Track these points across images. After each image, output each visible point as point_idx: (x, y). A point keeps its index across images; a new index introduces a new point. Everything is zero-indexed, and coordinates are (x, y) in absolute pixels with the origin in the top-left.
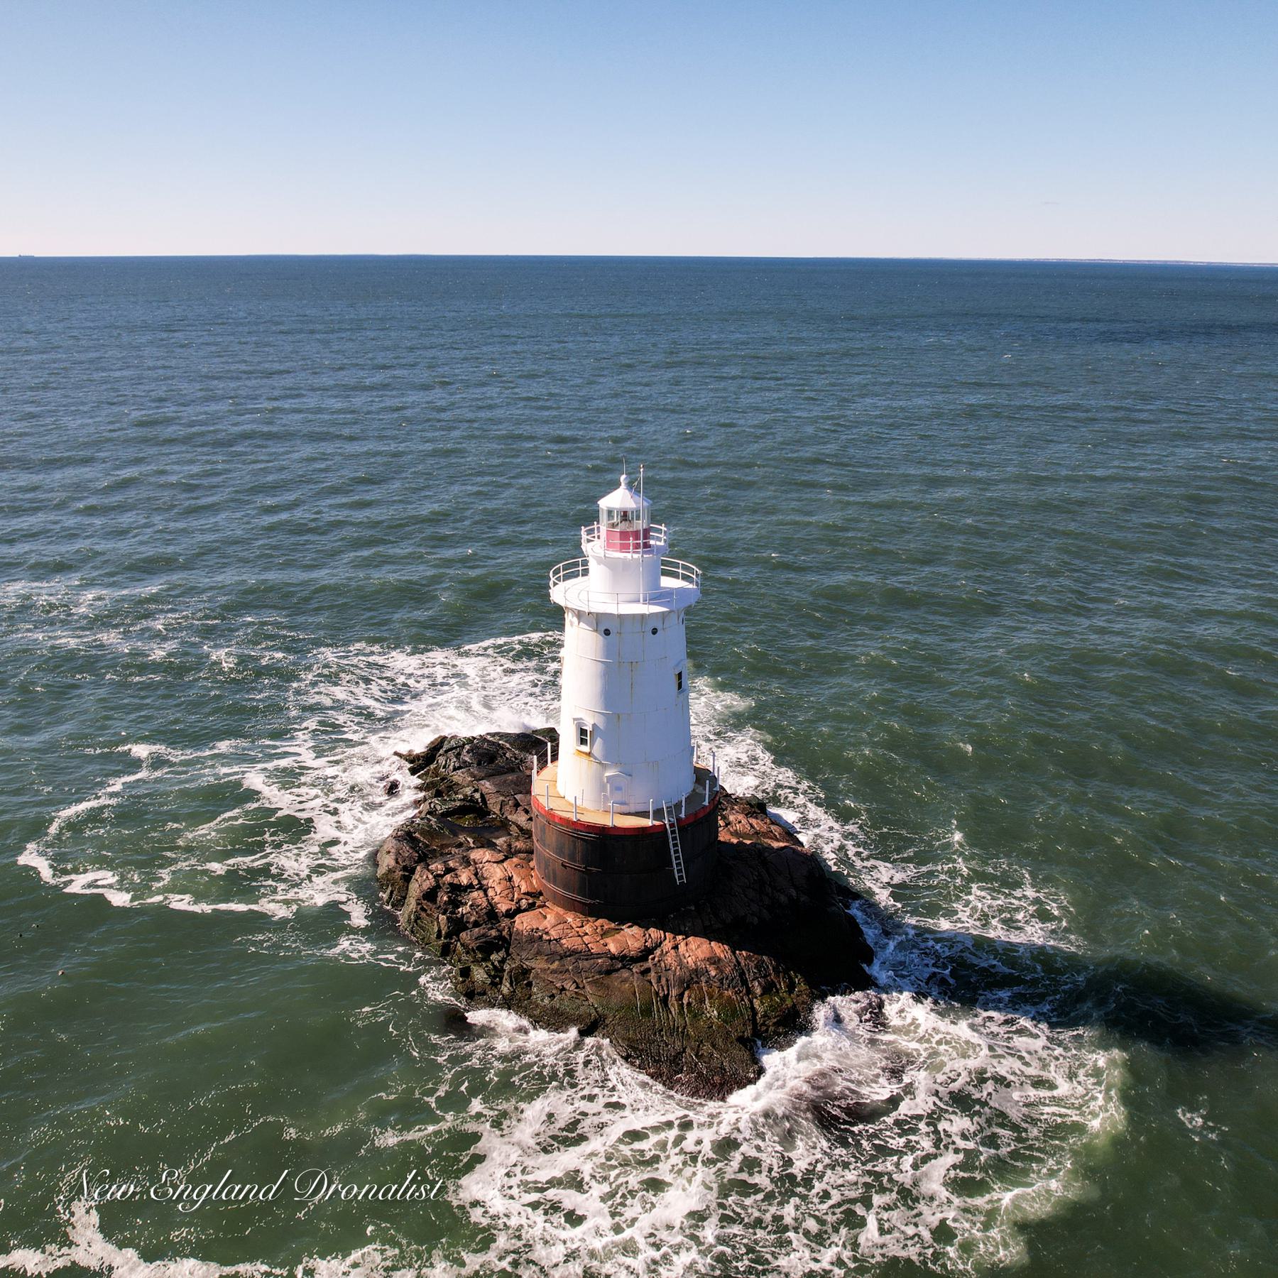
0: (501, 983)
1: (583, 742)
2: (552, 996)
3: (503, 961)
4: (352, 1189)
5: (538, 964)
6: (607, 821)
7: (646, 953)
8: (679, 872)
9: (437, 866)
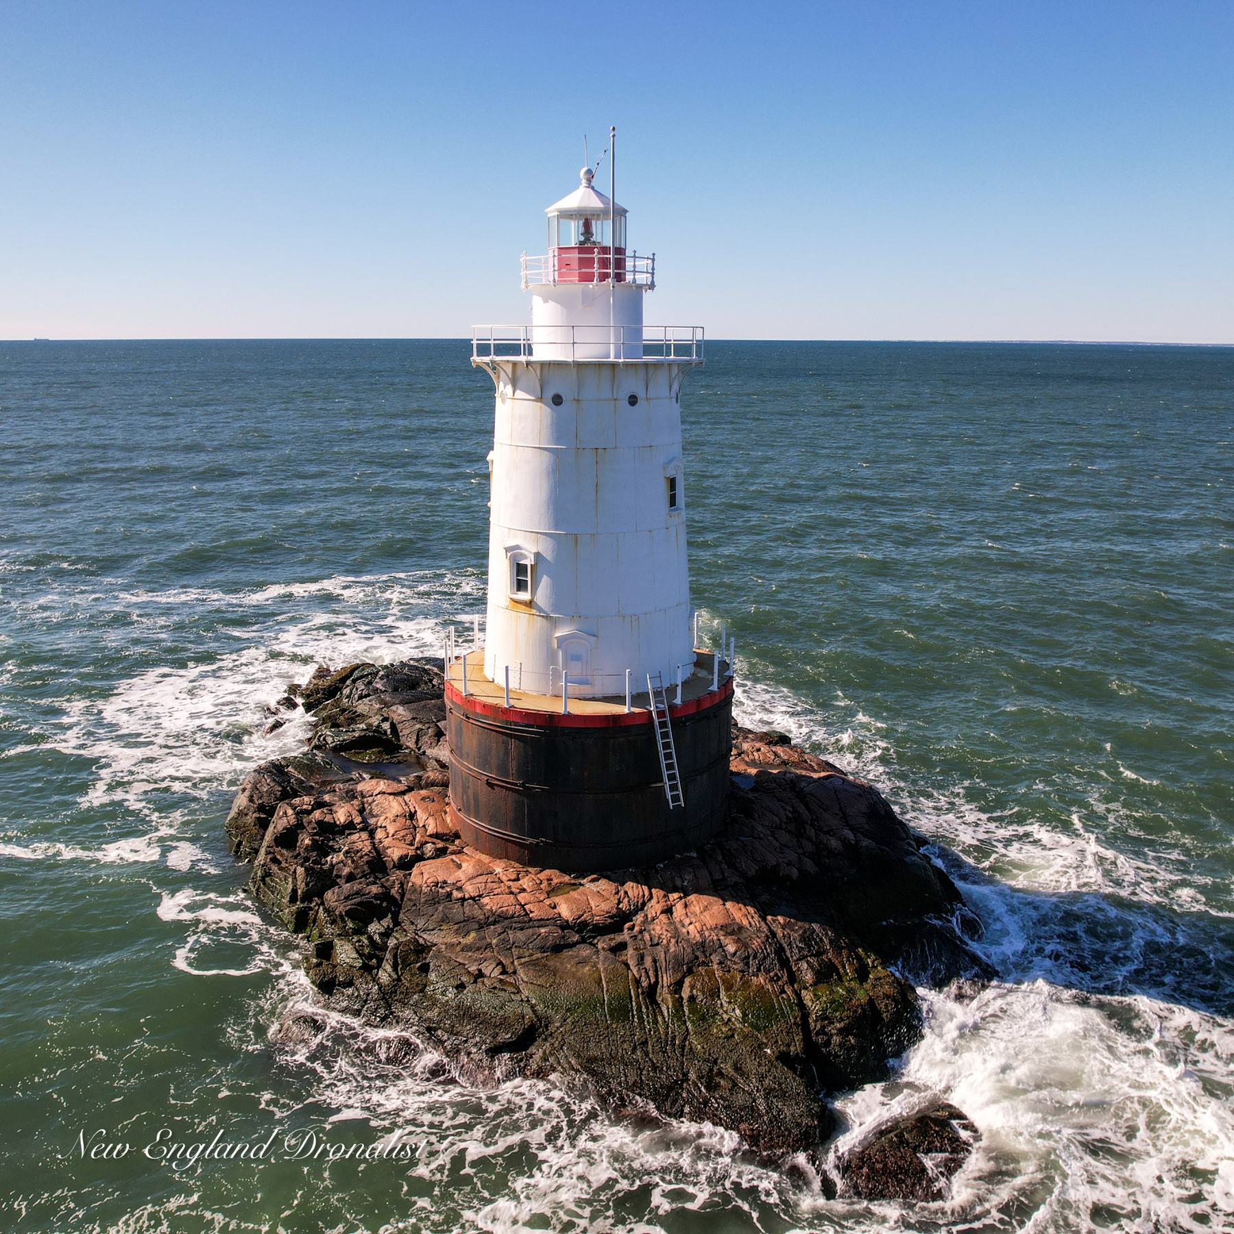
0: (379, 966)
1: (521, 585)
2: (461, 987)
3: (386, 934)
4: (340, 1147)
5: (439, 938)
6: (559, 708)
7: (619, 920)
8: (671, 789)
9: (306, 801)
